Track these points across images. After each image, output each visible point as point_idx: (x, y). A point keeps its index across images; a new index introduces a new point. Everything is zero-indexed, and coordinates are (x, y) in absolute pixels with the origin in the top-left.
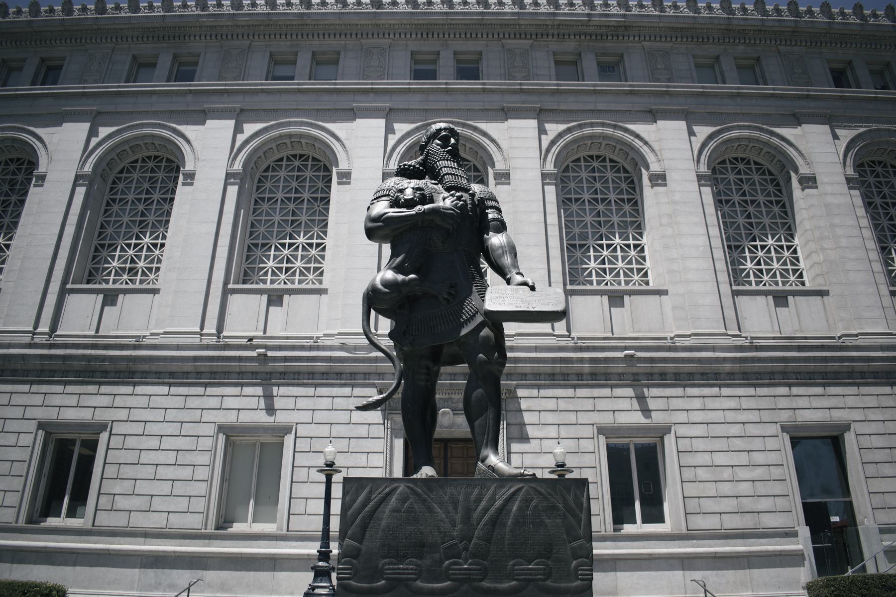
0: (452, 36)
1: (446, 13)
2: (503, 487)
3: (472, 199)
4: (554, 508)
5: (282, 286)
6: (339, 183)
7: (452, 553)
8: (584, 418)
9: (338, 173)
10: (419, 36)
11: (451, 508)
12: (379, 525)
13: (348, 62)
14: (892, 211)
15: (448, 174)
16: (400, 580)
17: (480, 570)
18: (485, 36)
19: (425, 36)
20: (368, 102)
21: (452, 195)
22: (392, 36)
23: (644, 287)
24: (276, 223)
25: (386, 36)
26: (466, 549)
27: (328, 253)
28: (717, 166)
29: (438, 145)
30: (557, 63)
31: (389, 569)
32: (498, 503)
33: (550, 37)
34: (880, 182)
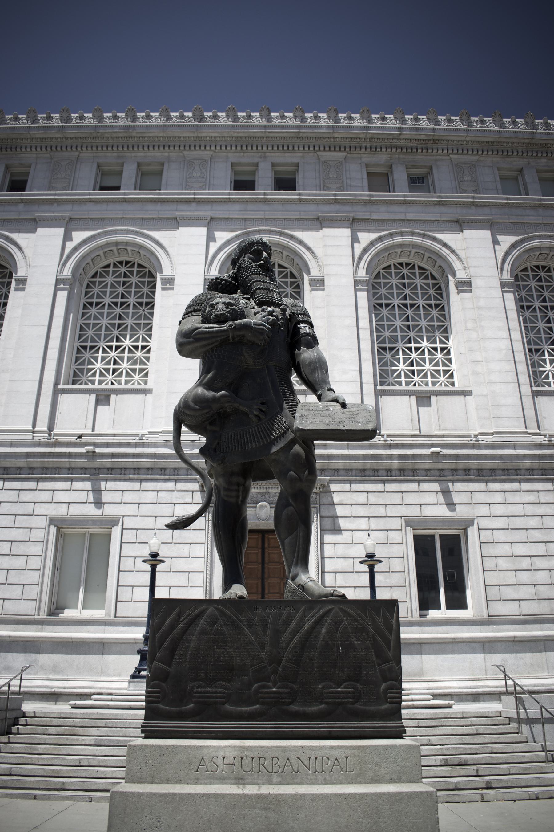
0: (270, 148)
1: (265, 127)
2: (311, 608)
3: (284, 310)
6: (163, 289)
8: (392, 511)
9: (162, 279)
10: (239, 148)
12: (188, 647)
13: (171, 174)
15: (259, 288)
18: (301, 149)
19: (244, 148)
20: (190, 211)
21: (263, 310)
22: (213, 148)
23: (450, 388)
25: (208, 148)
27: (152, 355)
28: (520, 274)
29: (250, 259)
30: (369, 174)
32: (307, 626)
33: (363, 150)
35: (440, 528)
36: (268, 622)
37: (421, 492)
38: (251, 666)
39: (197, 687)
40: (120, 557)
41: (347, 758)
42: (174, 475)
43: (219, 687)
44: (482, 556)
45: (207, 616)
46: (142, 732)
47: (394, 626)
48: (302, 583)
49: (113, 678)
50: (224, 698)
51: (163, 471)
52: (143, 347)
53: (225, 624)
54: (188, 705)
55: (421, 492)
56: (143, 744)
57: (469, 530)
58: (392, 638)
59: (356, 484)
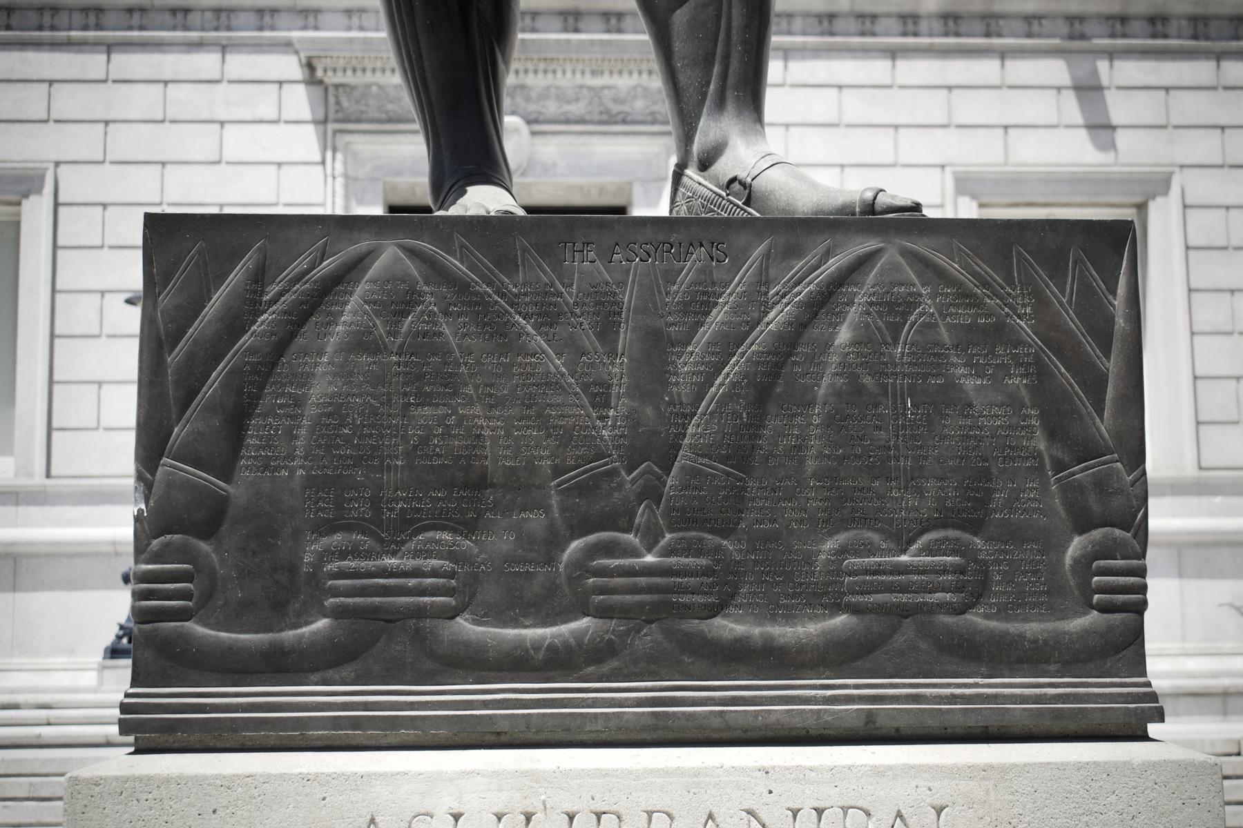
2: (794, 252)
4: (999, 333)
7: (594, 510)
11: (589, 340)
12: (299, 402)
16: (389, 619)
17: (707, 572)
26: (651, 493)
31: (342, 575)
32: (777, 318)
35: (1064, 200)
36: (619, 304)
37: (1011, 87)
38: (558, 471)
39: (343, 555)
40: (54, 291)
41: (939, 811)
42: (217, 29)
43: (429, 554)
44: (1190, 290)
45: (369, 281)
46: (125, 727)
47: (1120, 322)
48: (742, 175)
49: (50, 660)
50: (450, 592)
51: (180, 16)
53: (446, 313)
54: (308, 623)
55: (1011, 87)
56: (128, 772)
57: (1156, 211)
58: (1113, 366)
59: (803, 58)
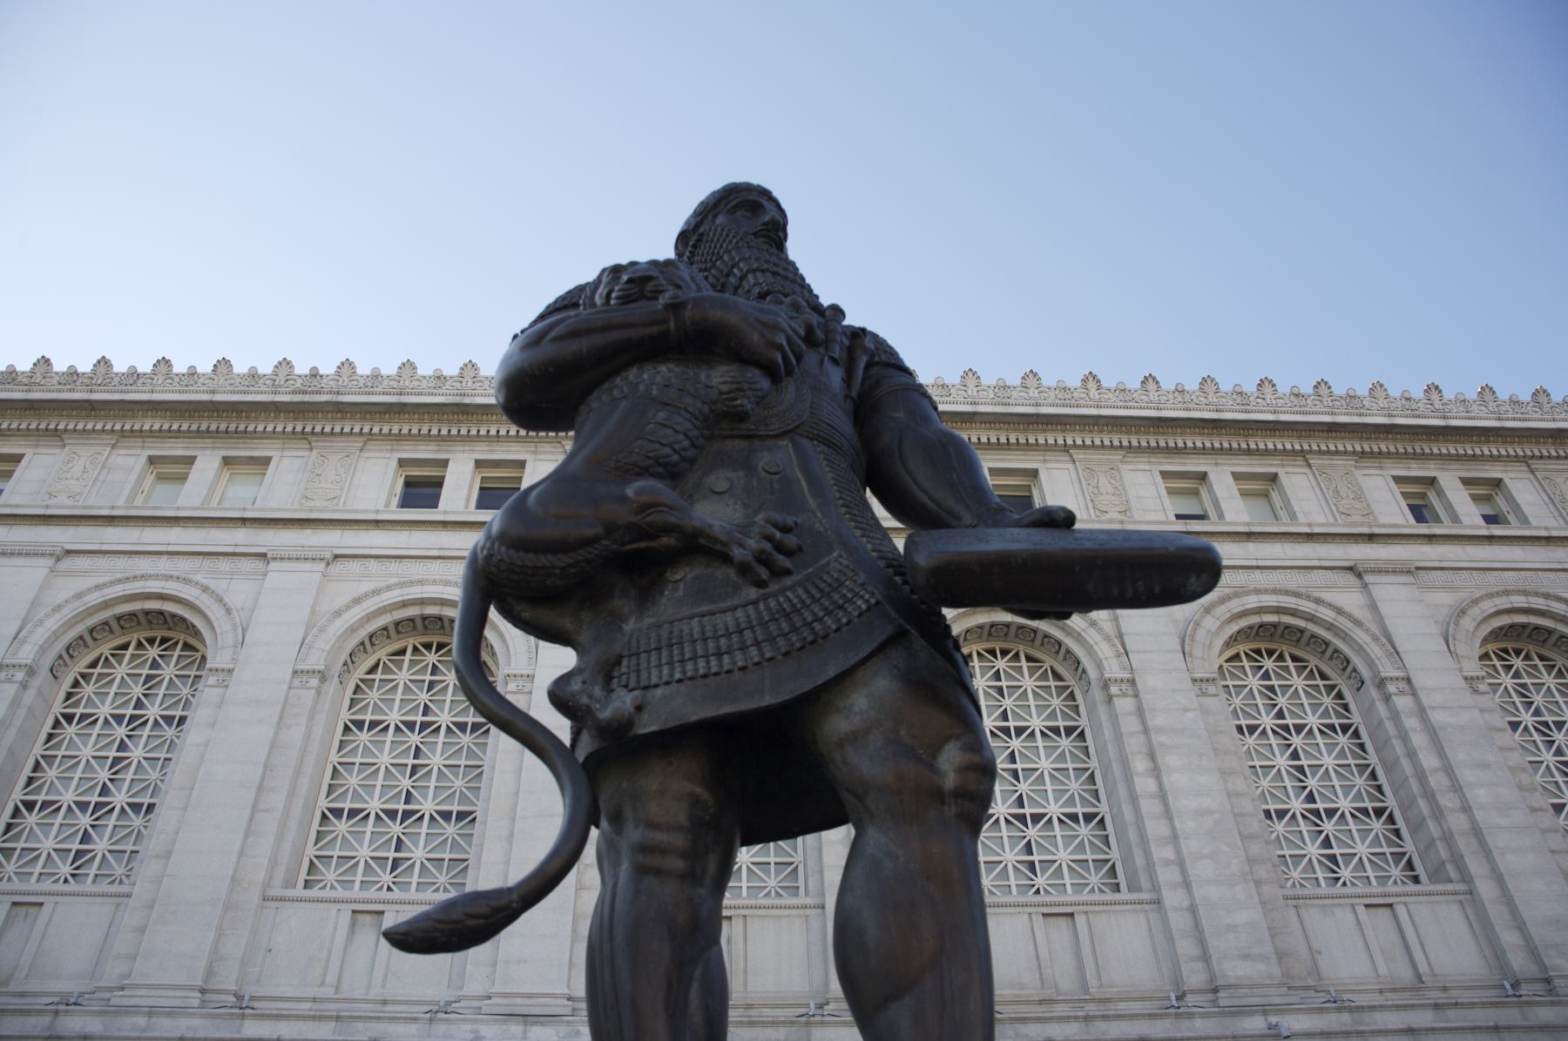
5: (384, 894)
14: (1559, 737)
24: (401, 686)
34: (1523, 686)
52: (461, 815)
